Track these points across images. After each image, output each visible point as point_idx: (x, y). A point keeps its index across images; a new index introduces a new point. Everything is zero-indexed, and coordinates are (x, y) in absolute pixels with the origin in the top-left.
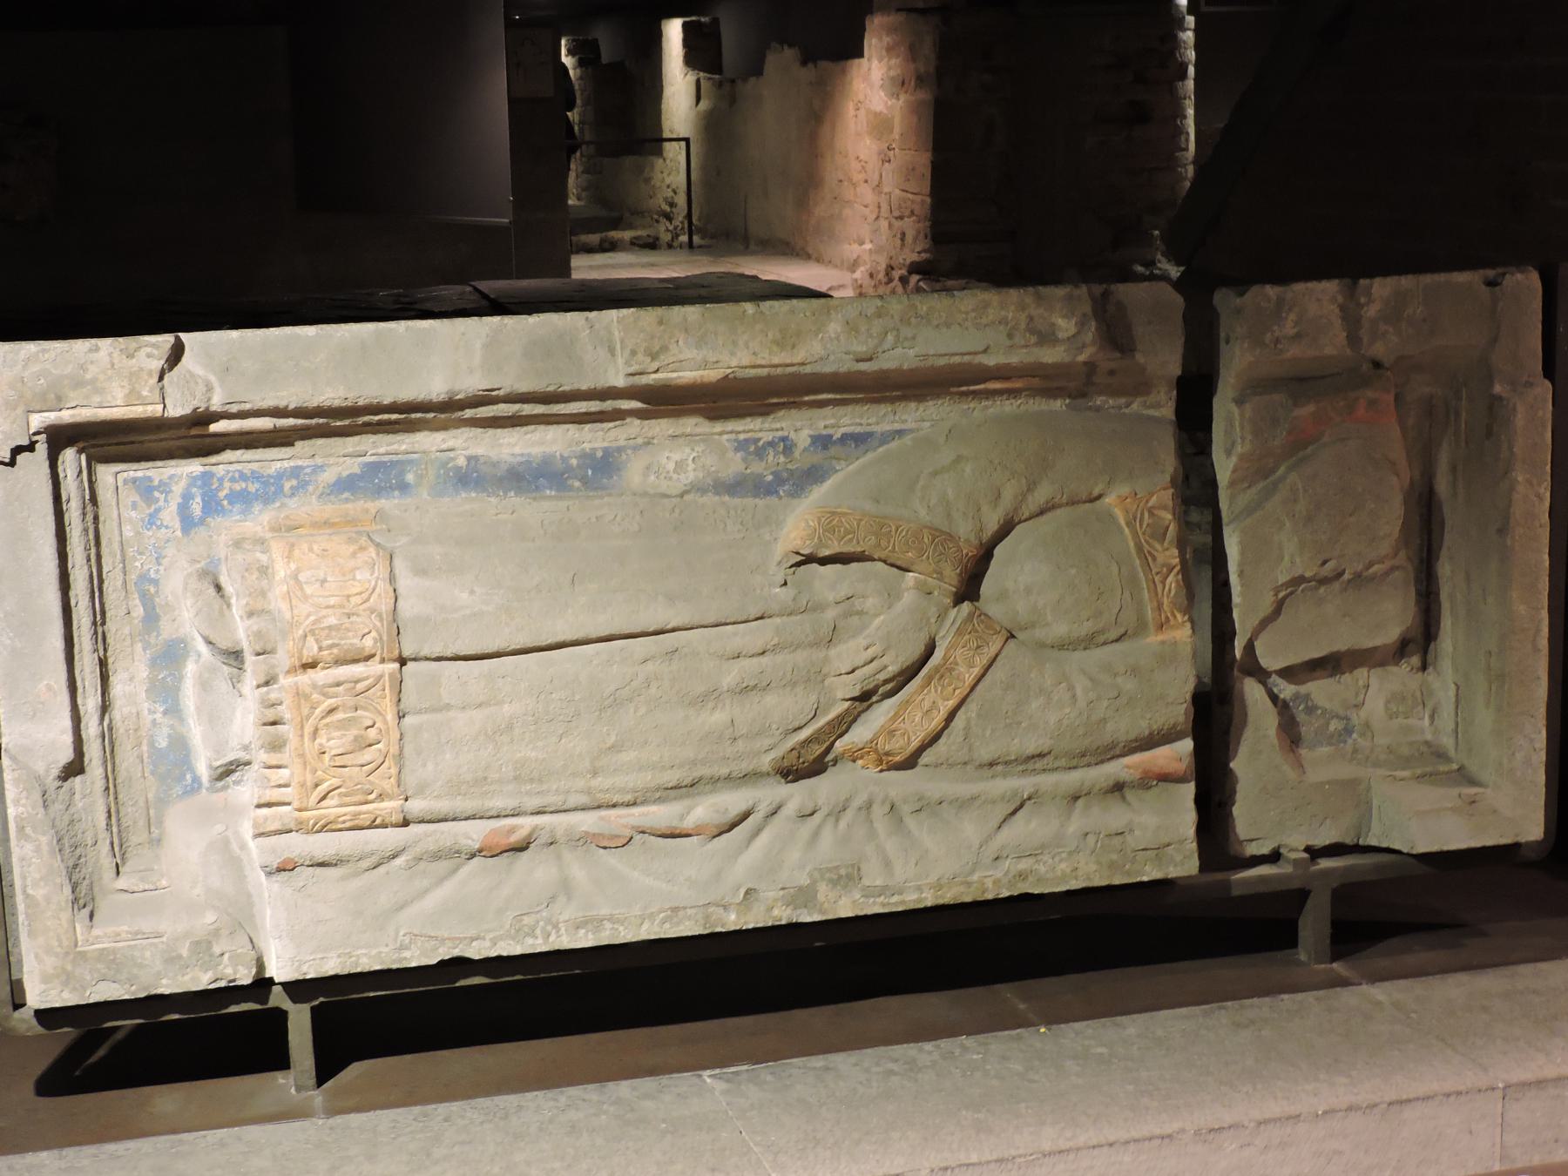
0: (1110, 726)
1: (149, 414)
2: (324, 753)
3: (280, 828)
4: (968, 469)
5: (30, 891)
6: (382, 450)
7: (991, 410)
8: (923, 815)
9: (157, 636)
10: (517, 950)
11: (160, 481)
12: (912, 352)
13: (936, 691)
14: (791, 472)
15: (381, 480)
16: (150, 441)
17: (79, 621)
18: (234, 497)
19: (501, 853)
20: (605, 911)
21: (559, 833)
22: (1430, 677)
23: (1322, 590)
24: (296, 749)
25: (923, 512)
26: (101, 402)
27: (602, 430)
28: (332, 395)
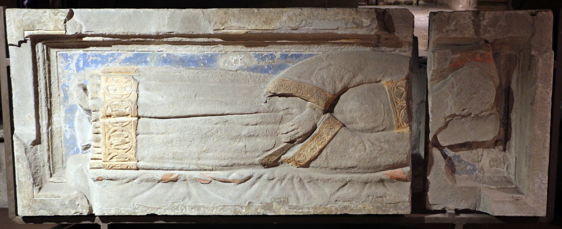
0: (378, 160)
1: (61, 33)
2: (112, 144)
3: (98, 166)
4: (332, 69)
5: (20, 179)
6: (140, 50)
7: (344, 49)
8: (311, 183)
9: (68, 103)
10: (172, 214)
11: (70, 55)
12: (311, 28)
13: (316, 142)
14: (273, 66)
15: (139, 59)
16: (66, 42)
17: (41, 97)
18: (92, 62)
19: (168, 182)
20: (201, 204)
21: (187, 177)
22: (507, 153)
23: (463, 119)
24: (103, 142)
25: (314, 82)
26: (46, 29)
27: (211, 48)
28: (119, 31)
